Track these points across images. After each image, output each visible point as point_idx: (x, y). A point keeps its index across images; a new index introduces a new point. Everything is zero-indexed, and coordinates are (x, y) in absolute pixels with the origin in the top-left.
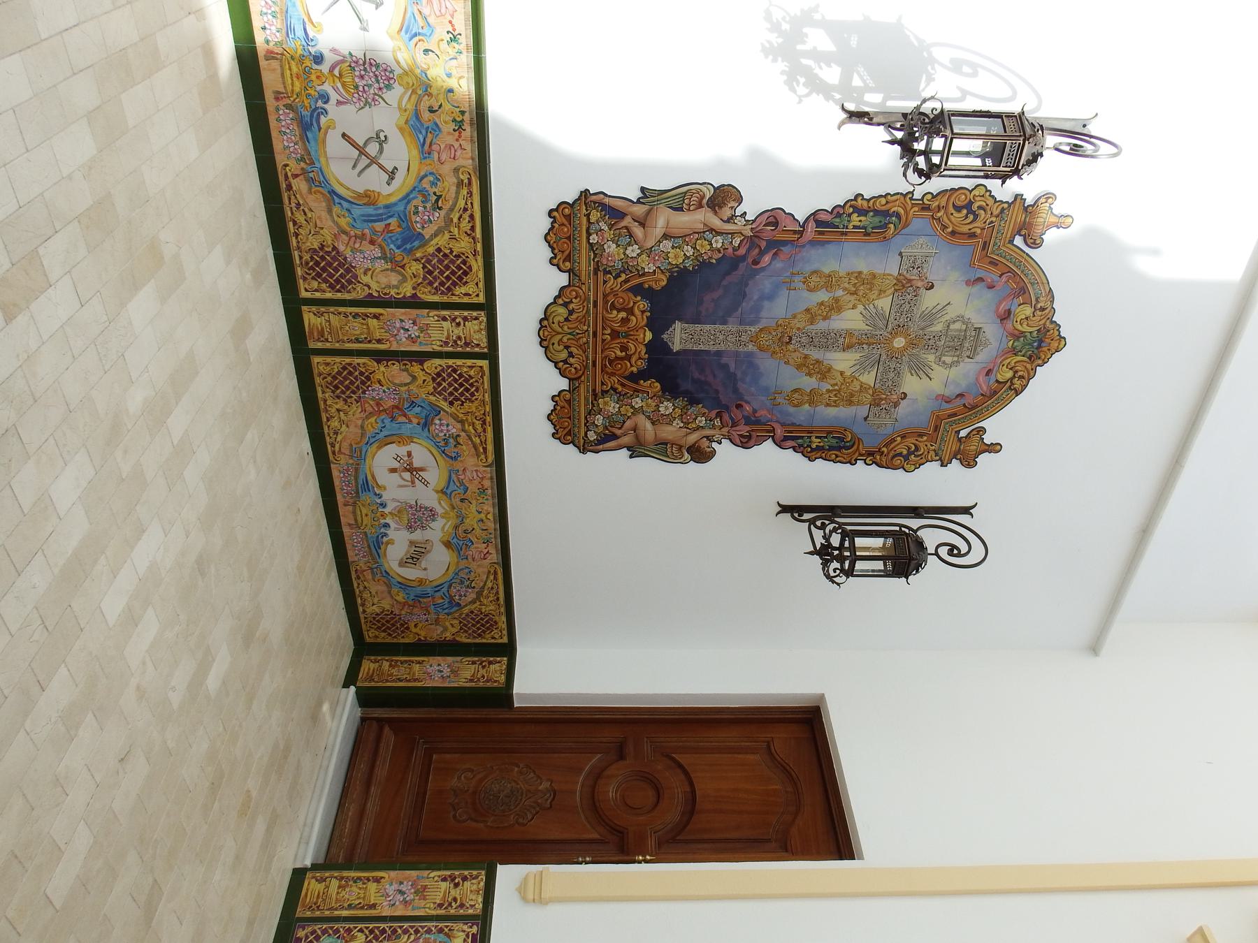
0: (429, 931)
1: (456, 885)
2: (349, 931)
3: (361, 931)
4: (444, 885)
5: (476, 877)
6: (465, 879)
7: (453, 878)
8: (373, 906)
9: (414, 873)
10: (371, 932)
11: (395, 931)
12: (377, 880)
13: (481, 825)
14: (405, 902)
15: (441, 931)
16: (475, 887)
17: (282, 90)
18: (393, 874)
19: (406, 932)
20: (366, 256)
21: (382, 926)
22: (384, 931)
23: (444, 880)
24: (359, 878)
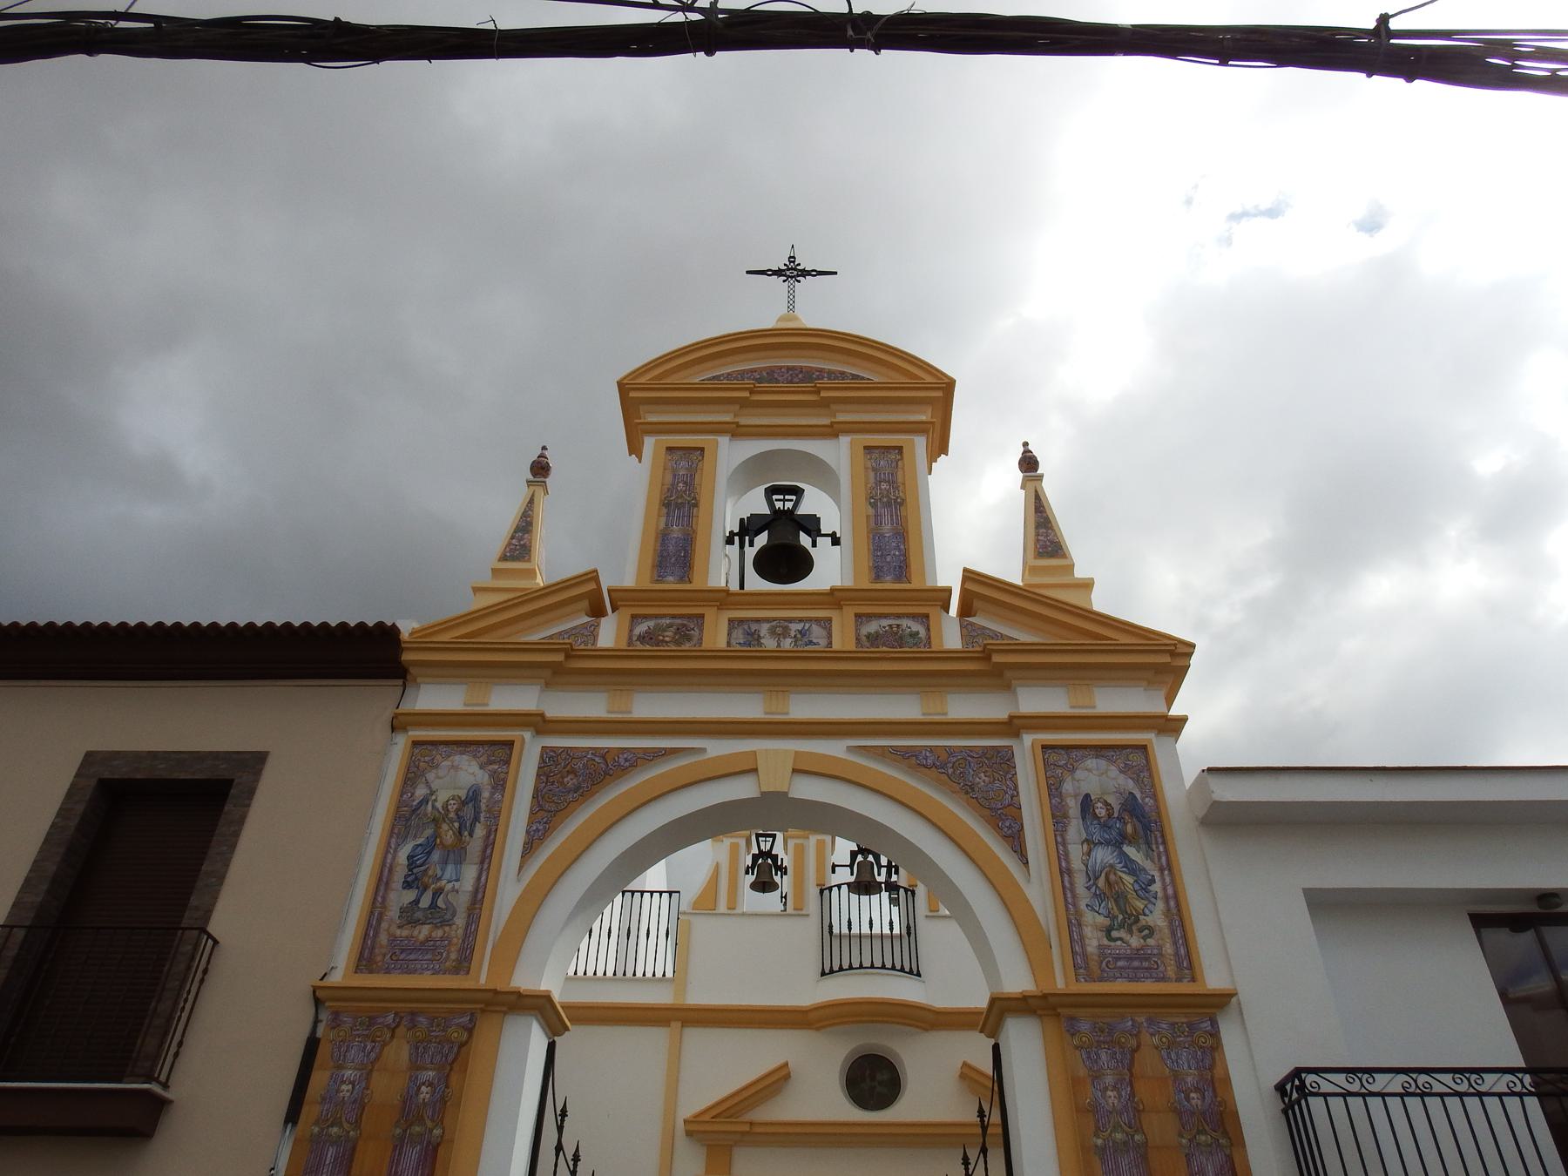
20: (823, 974)
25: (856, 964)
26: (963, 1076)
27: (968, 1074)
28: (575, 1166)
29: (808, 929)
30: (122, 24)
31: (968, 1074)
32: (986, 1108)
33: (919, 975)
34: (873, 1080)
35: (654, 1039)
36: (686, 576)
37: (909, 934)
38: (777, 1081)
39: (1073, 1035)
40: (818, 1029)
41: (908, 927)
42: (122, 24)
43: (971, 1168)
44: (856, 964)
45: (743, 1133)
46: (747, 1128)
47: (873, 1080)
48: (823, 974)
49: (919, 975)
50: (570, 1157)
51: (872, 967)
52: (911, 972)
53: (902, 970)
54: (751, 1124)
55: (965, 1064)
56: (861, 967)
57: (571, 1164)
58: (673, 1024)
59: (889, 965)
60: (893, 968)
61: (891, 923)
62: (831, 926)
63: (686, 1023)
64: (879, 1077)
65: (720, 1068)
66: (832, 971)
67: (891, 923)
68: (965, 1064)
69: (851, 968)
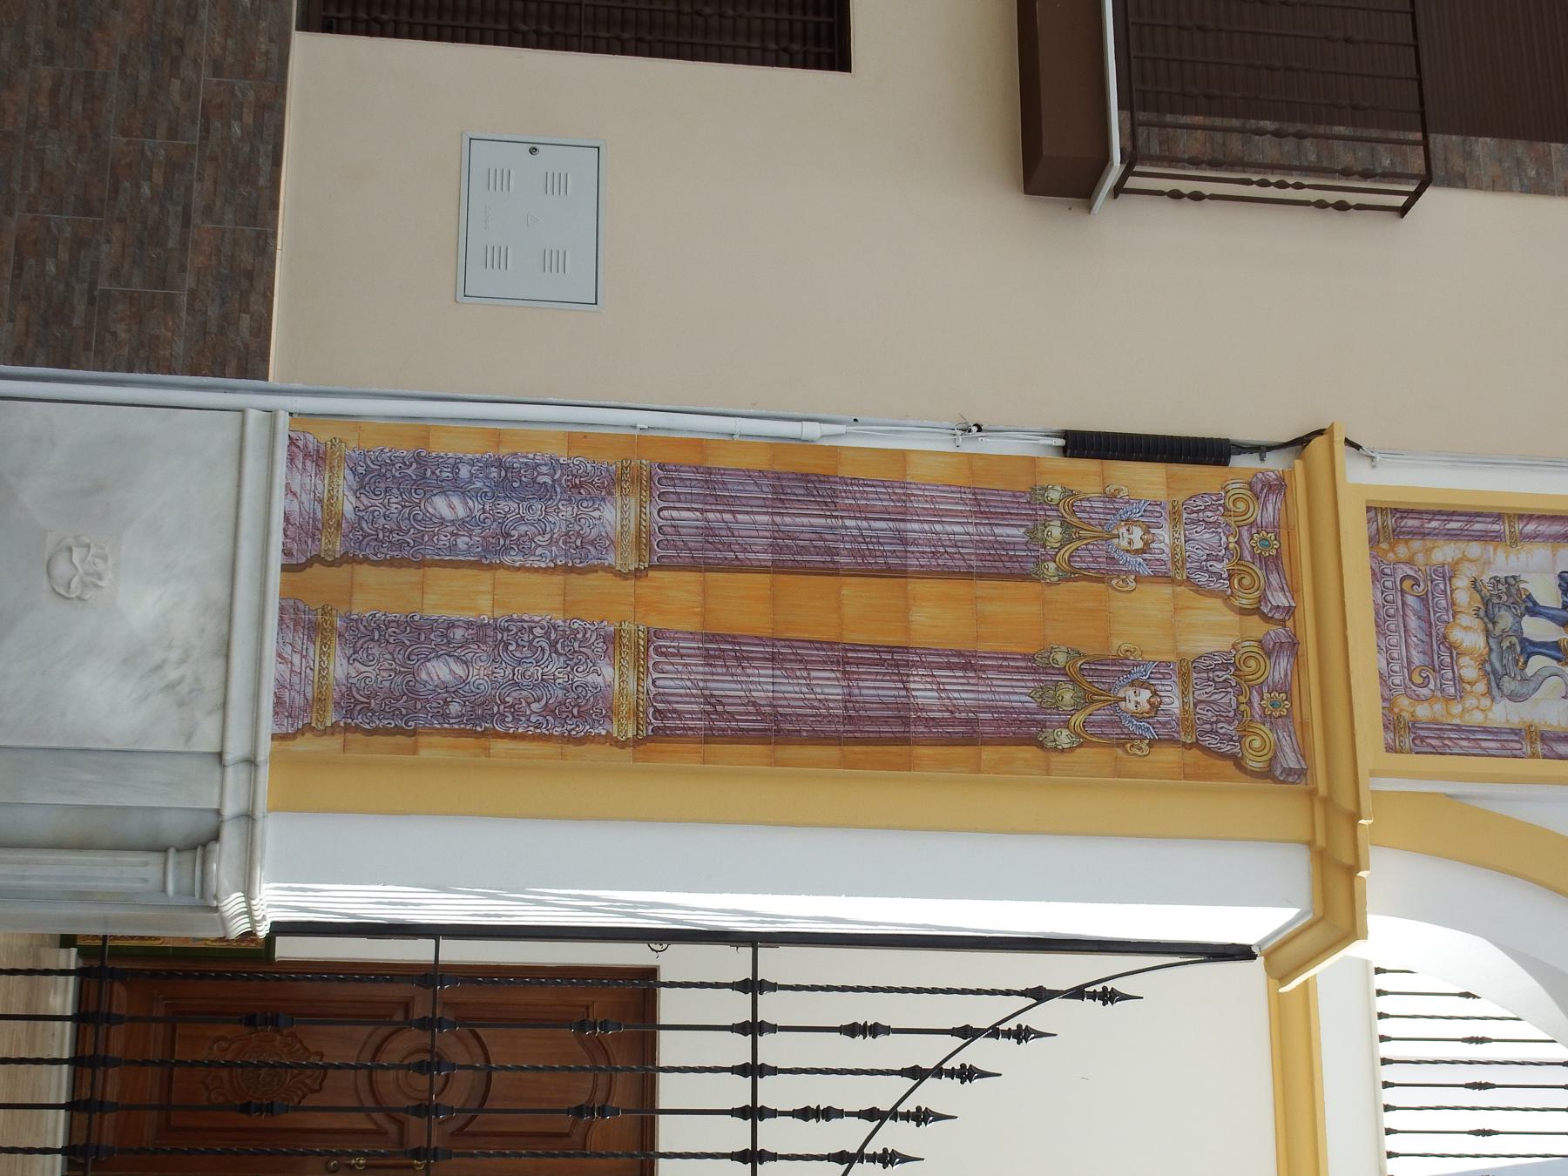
28: (1008, 1034)
50: (1024, 1020)
57: (1012, 1025)
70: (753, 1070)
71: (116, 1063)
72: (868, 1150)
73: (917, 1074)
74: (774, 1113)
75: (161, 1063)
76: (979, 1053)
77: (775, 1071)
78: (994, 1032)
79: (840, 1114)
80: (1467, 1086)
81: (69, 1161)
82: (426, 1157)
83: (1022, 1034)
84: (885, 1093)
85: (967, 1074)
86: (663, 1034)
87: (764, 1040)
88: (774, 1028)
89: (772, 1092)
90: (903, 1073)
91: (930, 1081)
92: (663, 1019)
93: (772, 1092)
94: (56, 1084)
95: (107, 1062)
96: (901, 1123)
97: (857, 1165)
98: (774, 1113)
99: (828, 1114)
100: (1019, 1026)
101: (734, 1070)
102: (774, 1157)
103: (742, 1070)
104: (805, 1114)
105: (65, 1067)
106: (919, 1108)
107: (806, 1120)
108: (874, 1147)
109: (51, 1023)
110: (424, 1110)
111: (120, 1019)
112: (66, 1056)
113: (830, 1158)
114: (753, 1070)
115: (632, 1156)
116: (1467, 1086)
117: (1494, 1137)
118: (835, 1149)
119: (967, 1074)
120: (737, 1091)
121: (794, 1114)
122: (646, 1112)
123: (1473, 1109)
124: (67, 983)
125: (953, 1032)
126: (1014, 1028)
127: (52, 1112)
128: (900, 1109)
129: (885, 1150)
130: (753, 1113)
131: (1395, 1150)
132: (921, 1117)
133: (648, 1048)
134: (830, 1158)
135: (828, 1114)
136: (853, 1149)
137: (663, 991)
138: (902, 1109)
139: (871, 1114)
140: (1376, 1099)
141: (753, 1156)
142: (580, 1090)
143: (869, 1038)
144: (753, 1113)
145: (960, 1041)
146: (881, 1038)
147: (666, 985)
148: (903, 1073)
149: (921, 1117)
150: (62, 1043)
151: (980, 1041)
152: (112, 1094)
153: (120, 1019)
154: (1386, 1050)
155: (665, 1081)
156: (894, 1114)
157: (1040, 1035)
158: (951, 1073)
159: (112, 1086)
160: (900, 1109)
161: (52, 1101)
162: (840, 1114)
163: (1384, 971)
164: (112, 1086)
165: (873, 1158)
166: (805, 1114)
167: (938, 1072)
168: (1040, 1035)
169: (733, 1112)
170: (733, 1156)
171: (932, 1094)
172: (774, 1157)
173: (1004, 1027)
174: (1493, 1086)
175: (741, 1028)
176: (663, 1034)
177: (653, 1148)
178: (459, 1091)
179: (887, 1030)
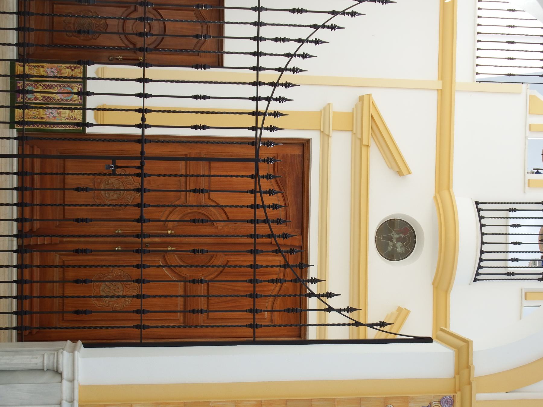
0: (64, 86)
1: (72, 70)
2: (36, 85)
3: (40, 85)
4: (68, 70)
5: (79, 68)
6: (75, 68)
7: (71, 67)
8: (42, 118)
9: (56, 65)
10: (44, 85)
11: (52, 86)
12: (43, 67)
13: (78, 39)
14: (54, 117)
15: (69, 86)
16: (79, 71)
17: (272, 173)
18: (48, 65)
19: (56, 86)
20: (477, 203)
21: (48, 84)
22: (48, 86)
23: (68, 68)
24: (36, 66)
25: (485, 230)
26: (400, 310)
27: (402, 313)
28: (348, 14)
29: (513, 193)
30: (56, 128)
31: (402, 313)
32: (386, 328)
33: (476, 280)
34: (397, 239)
35: (430, 72)
36: (532, 98)
37: (508, 274)
38: (399, 168)
39: (440, 402)
40: (435, 197)
41: (513, 274)
42: (56, 128)
43: (346, 313)
44: (485, 230)
45: (361, 139)
46: (365, 142)
47: (397, 239)
48: (477, 203)
49: (476, 280)
50: (354, 9)
51: (483, 243)
52: (478, 274)
53: (480, 267)
54: (368, 146)
55: (408, 312)
56: (483, 234)
57: (350, 11)
58: (441, 82)
59: (484, 256)
60: (481, 260)
61: (516, 260)
62: (515, 210)
63: (441, 92)
64: (399, 245)
65: (409, 123)
66: (479, 210)
67: (516, 260)
68: (408, 312)
69: (482, 226)
70: (258, 24)
71: (33, 30)
72: (298, 53)
73: (316, 27)
74: (265, 39)
75: (49, 15)
76: (337, 20)
77: (266, 24)
78: (344, 13)
79: (288, 40)
80: (506, 42)
81: (19, 143)
82: (141, 237)
83: (353, 14)
84: (304, 33)
85: (333, 27)
86: (226, 40)
87: (261, 58)
88: (266, 9)
89: (265, 32)
90: (311, 26)
91: (320, 30)
92: (226, 20)
93: (265, 32)
94: (12, 37)
95: (29, 29)
96: (310, 44)
97: (294, 58)
98: (265, 39)
99: (284, 40)
100: (352, 11)
101: (251, 54)
102: (265, 54)
103: (254, 24)
104: (276, 40)
105: (15, 160)
106: (316, 39)
107: (276, 42)
108: (300, 52)
109: (7, 311)
110: (142, 34)
111: (33, 14)
112: (15, 171)
113: (284, 55)
114: (258, 24)
115: (215, 52)
116: (506, 42)
117: (515, 12)
118: (286, 52)
119: (333, 27)
120: (252, 31)
121: (272, 40)
122: (220, 37)
123: (508, 50)
124: (13, 33)
125: (329, 12)
126: (351, 12)
127: (11, 31)
128: (309, 39)
129: (304, 53)
130: (258, 39)
131: (479, 64)
132: (317, 42)
133: (221, 30)
134: (284, 55)
135: (284, 40)
136: (293, 52)
137: (225, 55)
138: (310, 39)
139: (299, 41)
140: (474, 46)
141: (258, 9)
142: (198, 29)
143: (299, 14)
144: (258, 39)
145: (331, 16)
146: (304, 14)
147: (227, 23)
148: (311, 26)
149: (317, 42)
150: (13, 21)
151: (339, 16)
152: (32, 26)
153: (33, 14)
154: (479, 29)
155: (226, 42)
156: (307, 41)
157: (359, 14)
158: (328, 27)
159: (32, 37)
160: (309, 39)
161: (11, 27)
162: (288, 40)
163: (480, 49)
164: (32, 37)
165: (299, 56)
166: (276, 40)
167: (323, 26)
168: (359, 14)
169: (251, 9)
170: (251, 54)
171: (320, 34)
172: (265, 54)
173: (347, 11)
174: (516, 43)
175: (254, 54)
176: (226, 40)
177: (222, 50)
178: (156, 27)
179: (306, 11)
